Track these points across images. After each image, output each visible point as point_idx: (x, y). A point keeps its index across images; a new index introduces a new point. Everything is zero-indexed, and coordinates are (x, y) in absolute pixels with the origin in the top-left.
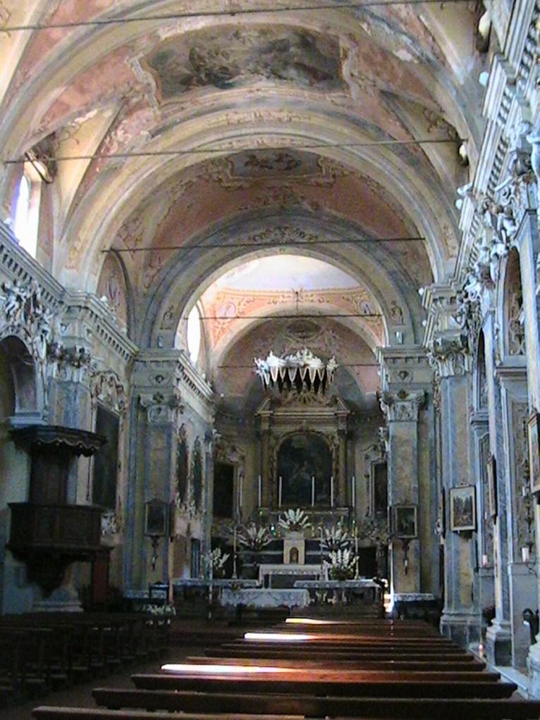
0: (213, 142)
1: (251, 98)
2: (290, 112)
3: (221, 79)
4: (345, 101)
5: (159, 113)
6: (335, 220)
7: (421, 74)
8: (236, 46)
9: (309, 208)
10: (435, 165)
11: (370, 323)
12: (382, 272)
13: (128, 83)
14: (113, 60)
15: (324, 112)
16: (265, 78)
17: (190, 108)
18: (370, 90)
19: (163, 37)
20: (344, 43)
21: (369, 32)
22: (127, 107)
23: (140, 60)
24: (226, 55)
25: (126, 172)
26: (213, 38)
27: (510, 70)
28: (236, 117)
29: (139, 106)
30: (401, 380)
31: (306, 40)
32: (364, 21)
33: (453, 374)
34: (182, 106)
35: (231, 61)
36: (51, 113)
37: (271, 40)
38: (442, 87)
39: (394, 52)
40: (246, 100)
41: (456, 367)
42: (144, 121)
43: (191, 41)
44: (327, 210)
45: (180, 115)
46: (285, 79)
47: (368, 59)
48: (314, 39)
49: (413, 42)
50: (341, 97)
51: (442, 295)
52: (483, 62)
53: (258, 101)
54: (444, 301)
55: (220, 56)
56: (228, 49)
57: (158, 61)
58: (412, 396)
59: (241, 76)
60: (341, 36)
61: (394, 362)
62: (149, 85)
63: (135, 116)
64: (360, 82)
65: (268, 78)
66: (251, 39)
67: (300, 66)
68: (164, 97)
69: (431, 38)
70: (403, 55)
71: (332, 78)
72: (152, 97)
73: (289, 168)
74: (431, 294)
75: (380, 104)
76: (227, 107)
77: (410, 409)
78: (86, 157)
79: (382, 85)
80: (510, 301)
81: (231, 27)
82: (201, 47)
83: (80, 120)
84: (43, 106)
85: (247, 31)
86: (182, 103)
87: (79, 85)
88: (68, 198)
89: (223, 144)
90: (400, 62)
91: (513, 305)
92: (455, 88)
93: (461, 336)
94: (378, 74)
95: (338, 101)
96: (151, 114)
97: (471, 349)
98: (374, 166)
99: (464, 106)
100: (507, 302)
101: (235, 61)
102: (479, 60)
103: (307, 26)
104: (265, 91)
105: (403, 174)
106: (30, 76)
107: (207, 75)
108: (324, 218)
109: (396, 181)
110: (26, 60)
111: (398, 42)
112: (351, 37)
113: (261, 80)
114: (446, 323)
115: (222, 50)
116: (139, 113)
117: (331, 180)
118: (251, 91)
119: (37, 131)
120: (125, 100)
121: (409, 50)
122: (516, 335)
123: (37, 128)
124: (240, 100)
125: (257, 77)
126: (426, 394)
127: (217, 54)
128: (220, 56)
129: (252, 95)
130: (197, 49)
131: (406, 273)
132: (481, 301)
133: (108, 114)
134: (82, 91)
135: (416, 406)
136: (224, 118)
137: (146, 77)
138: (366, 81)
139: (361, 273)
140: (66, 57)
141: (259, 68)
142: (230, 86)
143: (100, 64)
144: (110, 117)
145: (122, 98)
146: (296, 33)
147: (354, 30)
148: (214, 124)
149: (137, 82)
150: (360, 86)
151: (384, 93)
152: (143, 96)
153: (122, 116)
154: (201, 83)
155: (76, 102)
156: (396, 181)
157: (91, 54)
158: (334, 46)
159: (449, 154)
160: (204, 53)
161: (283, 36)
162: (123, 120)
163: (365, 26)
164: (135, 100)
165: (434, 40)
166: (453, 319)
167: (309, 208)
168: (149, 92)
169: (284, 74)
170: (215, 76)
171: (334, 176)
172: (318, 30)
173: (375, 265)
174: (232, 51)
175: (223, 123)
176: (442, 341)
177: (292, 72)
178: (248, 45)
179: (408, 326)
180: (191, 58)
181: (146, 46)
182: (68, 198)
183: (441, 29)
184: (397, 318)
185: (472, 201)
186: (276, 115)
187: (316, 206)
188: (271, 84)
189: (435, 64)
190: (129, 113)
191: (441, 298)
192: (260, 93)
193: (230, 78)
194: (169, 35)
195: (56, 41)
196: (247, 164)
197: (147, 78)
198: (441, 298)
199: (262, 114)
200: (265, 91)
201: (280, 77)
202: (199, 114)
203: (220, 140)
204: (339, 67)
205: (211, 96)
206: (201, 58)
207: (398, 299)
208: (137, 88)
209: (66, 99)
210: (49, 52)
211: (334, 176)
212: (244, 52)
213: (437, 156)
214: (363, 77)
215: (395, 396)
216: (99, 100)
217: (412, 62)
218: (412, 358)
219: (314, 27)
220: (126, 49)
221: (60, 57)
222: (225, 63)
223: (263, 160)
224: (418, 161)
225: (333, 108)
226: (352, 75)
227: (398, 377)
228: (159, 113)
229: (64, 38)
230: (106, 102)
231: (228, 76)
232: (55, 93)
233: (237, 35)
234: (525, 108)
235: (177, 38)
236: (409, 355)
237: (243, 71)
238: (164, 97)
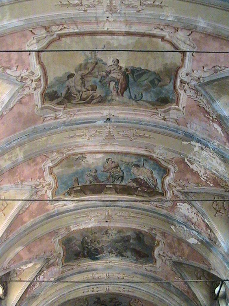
0: (85, 287)
1: (105, 266)
2: (124, 274)
3: (93, 254)
4: (153, 269)
5: (61, 269)
13: (51, 252)
14: (48, 238)
17: (76, 269)
18: (168, 262)
21: (175, 231)
22: (48, 264)
24: (99, 243)
25: (40, 299)
28: (97, 276)
29: (53, 265)
31: (139, 236)
32: (173, 224)
34: (73, 267)
36: (14, 260)
37: (122, 236)
39: (187, 240)
40: (103, 267)
42: (54, 273)
43: (85, 233)
45: (70, 272)
46: (124, 257)
47: (170, 246)
48: (143, 236)
49: (198, 234)
50: (150, 266)
57: (67, 242)
59: (104, 254)
60: (158, 234)
63: (50, 269)
64: (163, 258)
67: (134, 251)
68: (65, 262)
69: (209, 231)
70: (192, 241)
71: (148, 256)
72: (60, 261)
75: (172, 269)
76: (94, 270)
78: (29, 281)
79: (175, 258)
81: (105, 227)
82: (88, 237)
83: (24, 267)
84: (11, 255)
86: (73, 265)
87: (29, 248)
88: (138, 129)
89: (90, 288)
90: (188, 244)
92: (222, 255)
96: (58, 270)
104: (113, 263)
106: (9, 238)
107: (88, 252)
110: (10, 229)
111: (190, 234)
112: (163, 234)
113: (113, 256)
115: (98, 239)
116: (52, 268)
118: (107, 263)
119: (6, 268)
120: (48, 260)
121: (196, 238)
123: (6, 266)
124: (100, 267)
127: (95, 241)
129: (106, 265)
130: (86, 238)
133: (39, 266)
134: (30, 251)
136: (91, 276)
137: (59, 249)
140: (28, 231)
141: (113, 250)
142: (97, 259)
143: (41, 239)
144: (40, 268)
145: (47, 259)
146: (135, 233)
148: (85, 278)
149: (55, 252)
150: (162, 260)
151: (175, 263)
152: (56, 259)
153: (44, 268)
154: (84, 256)
155: (26, 257)
157: (40, 232)
158: (153, 239)
160: (89, 241)
161: (128, 234)
162: (44, 270)
163: (173, 227)
164: (52, 261)
165: (211, 231)
169: (124, 254)
170: (91, 253)
172: (146, 231)
174: (102, 240)
175: (91, 278)
177: (129, 253)
178: (111, 238)
180: (82, 242)
181: (63, 233)
182: (138, 129)
183: (214, 225)
188: (117, 259)
190: (48, 267)
192: (111, 264)
193: (97, 255)
194: (75, 229)
195: (25, 223)
196: (95, 302)
199: (110, 274)
201: (122, 256)
202: (80, 273)
203: (89, 286)
204: (153, 250)
205: (87, 263)
206: (87, 243)
208: (55, 254)
209: (22, 254)
210: (21, 227)
214: (165, 255)
216: (36, 258)
217: (197, 244)
219: (145, 229)
220: (53, 233)
221: (25, 231)
226: (159, 254)
228: (61, 269)
229: (29, 222)
230: (39, 259)
231: (97, 253)
232: (19, 249)
233: (106, 232)
235: (78, 231)
237: (105, 252)
238: (65, 262)
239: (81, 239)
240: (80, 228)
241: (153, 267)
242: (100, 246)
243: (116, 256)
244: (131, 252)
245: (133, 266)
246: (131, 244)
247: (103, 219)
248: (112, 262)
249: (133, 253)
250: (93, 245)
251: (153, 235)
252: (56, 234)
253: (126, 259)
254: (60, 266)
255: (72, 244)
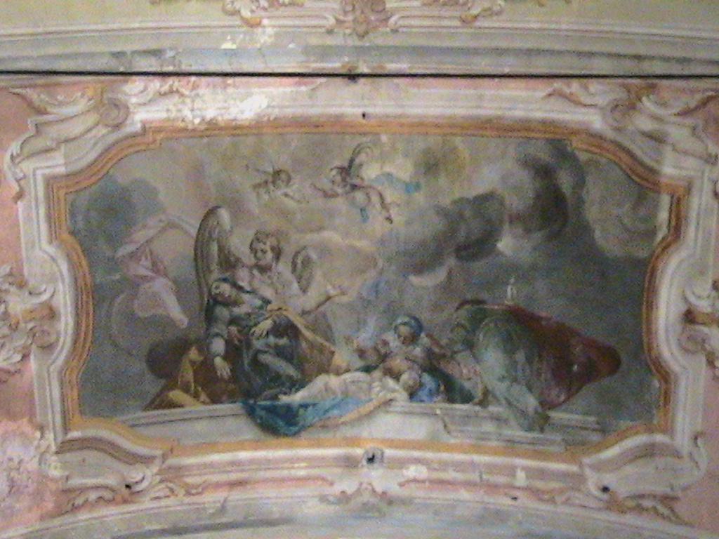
19: (140, 117)
23: (50, 182)
55: (283, 267)
59: (334, 381)
62: (52, 314)
67: (524, 329)
81: (338, 125)
97: (665, 200)
107: (233, 352)
118: (349, 463)
127: (278, 253)
128: (283, 267)
154: (210, 387)
160: (239, 244)
168: (48, 348)
177: (489, 365)
178: (377, 225)
192: (378, 478)
197: (52, 279)
201: (452, 391)
206: (229, 263)
222: (297, 303)
223: (196, 339)
237: (342, 356)
239: (192, 226)
240: (187, 113)
241: (649, 452)
242: (312, 298)
243: (412, 395)
244: (509, 346)
245: (521, 479)
246: (512, 269)
247: (330, 32)
248: (389, 452)
249: (520, 356)
250: (268, 293)
251: (641, 149)
252: (31, 121)
253: (467, 418)
254: (50, 436)
255: (133, 256)
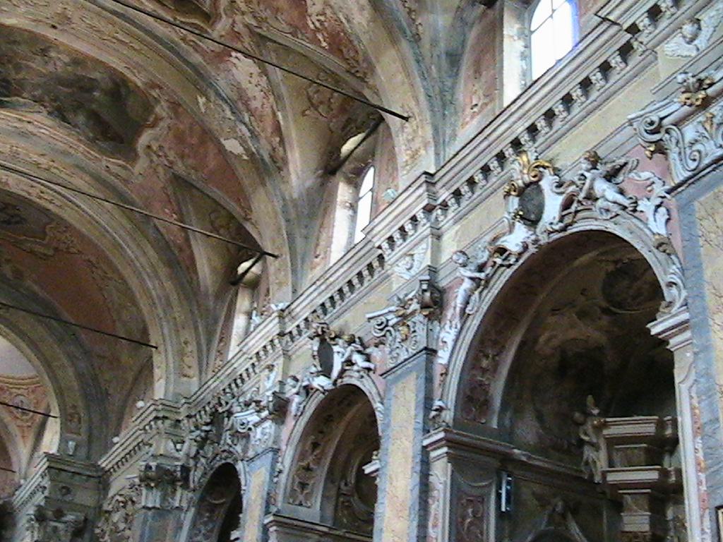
4: (123, 173)
6: (34, 297)
7: (245, 175)
8: (37, 64)
9: (9, 275)
10: (200, 274)
11: (19, 422)
12: (70, 372)
15: (92, 175)
16: (45, 113)
20: (161, 110)
24: (18, 68)
26: (15, 42)
27: (433, 196)
30: (59, 497)
31: (119, 88)
33: (158, 506)
35: (20, 76)
38: (267, 193)
39: (222, 140)
41: (164, 499)
44: (29, 283)
47: (180, 138)
48: (130, 92)
51: (167, 415)
52: (322, 184)
53: (24, 135)
54: (168, 422)
56: (25, 62)
58: (70, 517)
61: (58, 475)
64: (155, 158)
65: (49, 113)
66: (58, 63)
67: (94, 117)
70: (232, 146)
71: (122, 142)
73: (9, 223)
74: (155, 410)
77: (62, 533)
79: (180, 168)
80: (304, 445)
85: (59, 52)
90: (221, 150)
91: (307, 448)
93: (308, 484)
94: (182, 157)
95: (114, 169)
98: (126, 252)
99: (288, 221)
100: (301, 444)
101: (24, 79)
102: (319, 180)
103: (129, 75)
104: (36, 126)
105: (156, 272)
108: (22, 290)
109: (146, 277)
111: (233, 129)
112: (175, 106)
114: (162, 447)
117: (51, 252)
121: (243, 142)
122: (300, 483)
125: (37, 107)
126: (86, 520)
131: (95, 378)
132: (252, 434)
135: (71, 530)
138: (163, 159)
139: (48, 364)
147: (185, 98)
156: (146, 277)
158: (148, 107)
159: (219, 266)
161: (96, 75)
163: (202, 100)
166: (171, 445)
167: (9, 275)
169: (70, 116)
171: (56, 249)
172: (139, 84)
173: (65, 361)
174: (28, 67)
176: (157, 467)
178: (51, 68)
179: (84, 437)
183: (293, 132)
184: (73, 425)
185: (279, 322)
186: (35, 158)
187: (19, 275)
188: (49, 122)
189: (268, 167)
191: (165, 418)
198: (165, 418)
200: (36, 126)
201: (64, 119)
204: (138, 132)
207: (80, 404)
211: (56, 249)
212: (42, 75)
213: (206, 265)
215: (50, 514)
217: (238, 157)
218: (79, 474)
222: (13, 75)
224: (178, 262)
225: (104, 174)
226: (149, 147)
227: (58, 493)
233: (44, 52)
234: (435, 240)
236: (77, 470)
237: (25, 95)
